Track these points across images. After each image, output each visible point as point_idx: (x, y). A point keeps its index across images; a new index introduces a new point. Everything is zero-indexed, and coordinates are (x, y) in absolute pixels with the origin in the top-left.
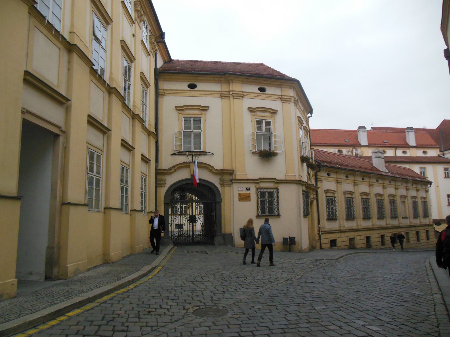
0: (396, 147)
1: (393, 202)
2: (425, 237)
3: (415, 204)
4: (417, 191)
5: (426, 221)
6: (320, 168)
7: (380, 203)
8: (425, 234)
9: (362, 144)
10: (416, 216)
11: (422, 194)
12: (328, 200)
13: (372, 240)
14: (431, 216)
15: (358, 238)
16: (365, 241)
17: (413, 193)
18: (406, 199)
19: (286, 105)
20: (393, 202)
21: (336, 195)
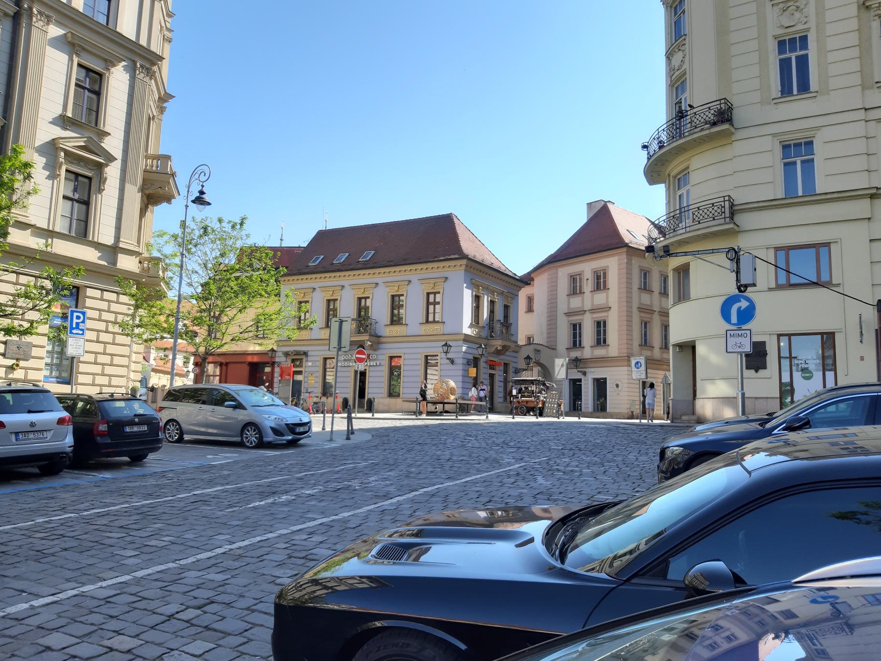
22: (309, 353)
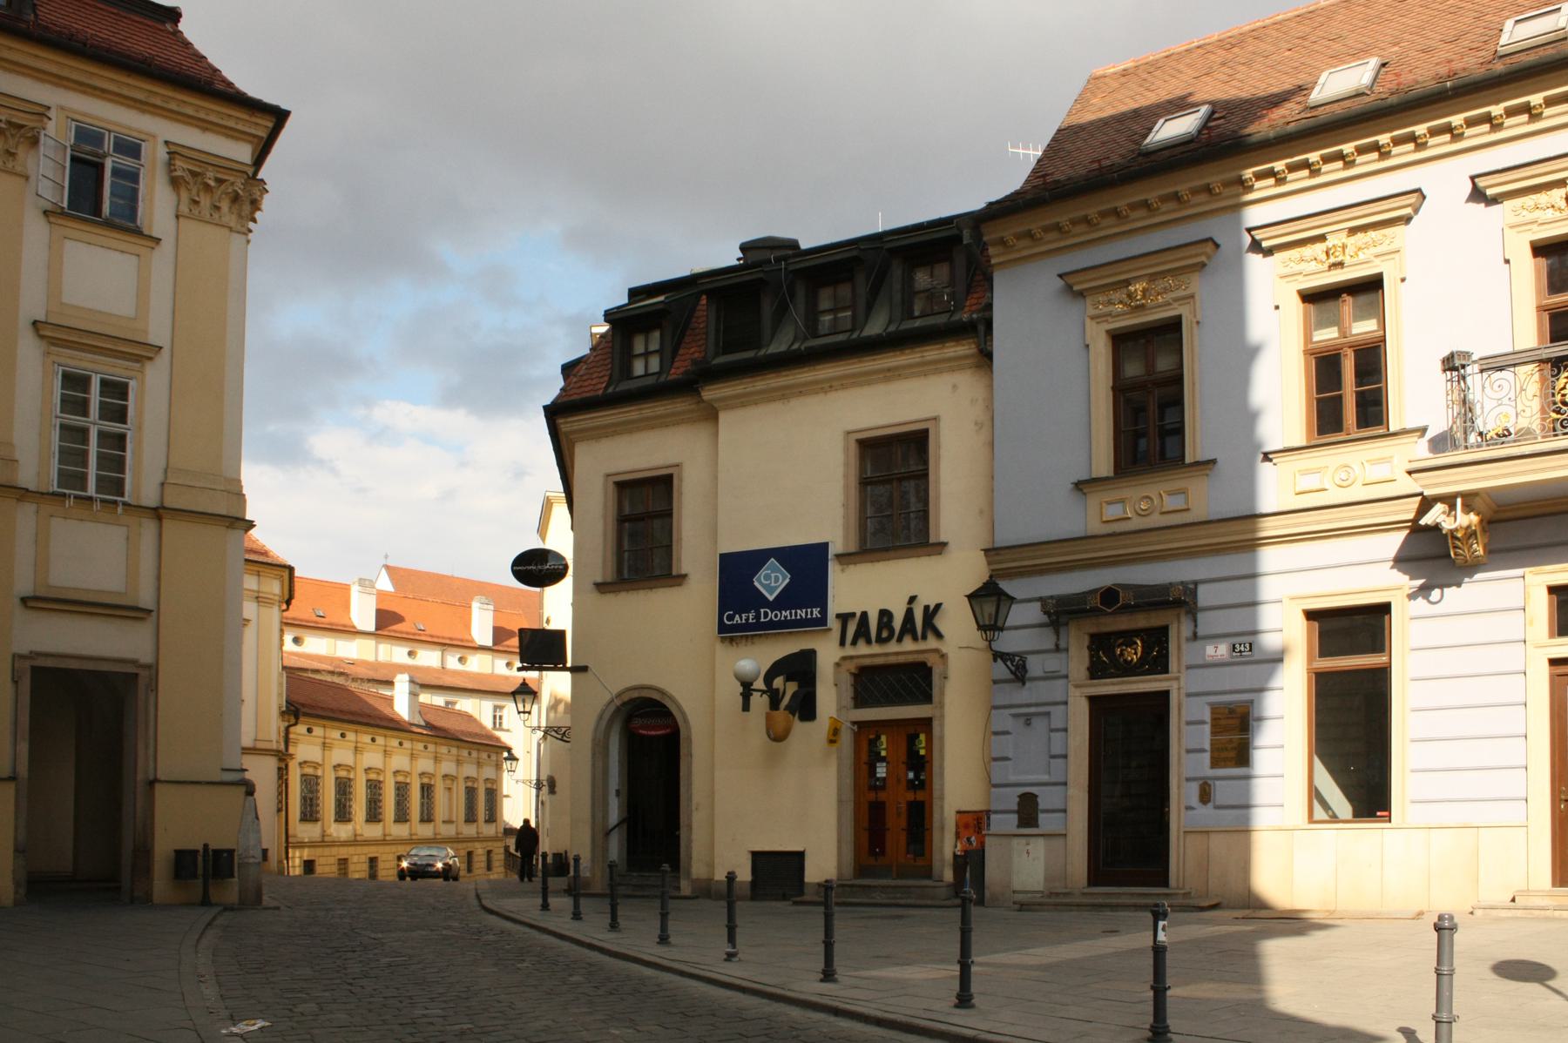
0: (445, 645)
1: (427, 790)
2: (484, 865)
3: (471, 793)
4: (479, 764)
5: (489, 830)
6: (297, 718)
7: (374, 787)
8: (484, 858)
9: (360, 627)
10: (470, 818)
11: (488, 772)
12: (398, 789)
13: (381, 865)
14: (134, 662)
15: (355, 859)
16: (366, 867)
17: (469, 770)
18: (535, 707)
19: (264, 610)
20: (427, 790)
21: (319, 773)
22: (1205, 596)
